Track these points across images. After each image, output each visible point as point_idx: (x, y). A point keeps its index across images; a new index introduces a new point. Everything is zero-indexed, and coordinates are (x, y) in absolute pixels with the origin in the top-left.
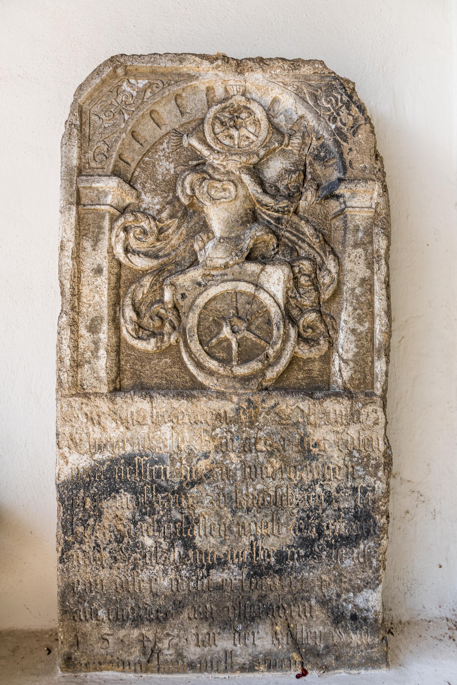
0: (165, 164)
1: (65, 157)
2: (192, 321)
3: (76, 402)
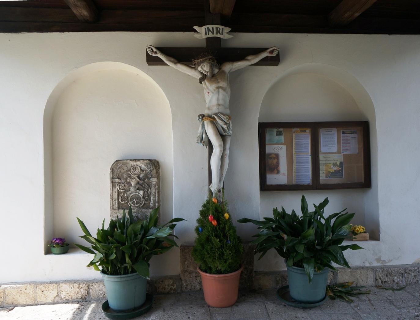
0: (125, 175)
1: (110, 176)
2: (129, 199)
3: (113, 211)
